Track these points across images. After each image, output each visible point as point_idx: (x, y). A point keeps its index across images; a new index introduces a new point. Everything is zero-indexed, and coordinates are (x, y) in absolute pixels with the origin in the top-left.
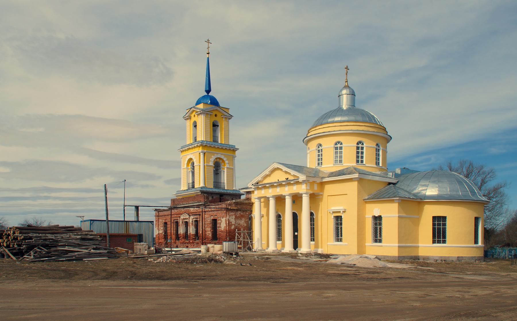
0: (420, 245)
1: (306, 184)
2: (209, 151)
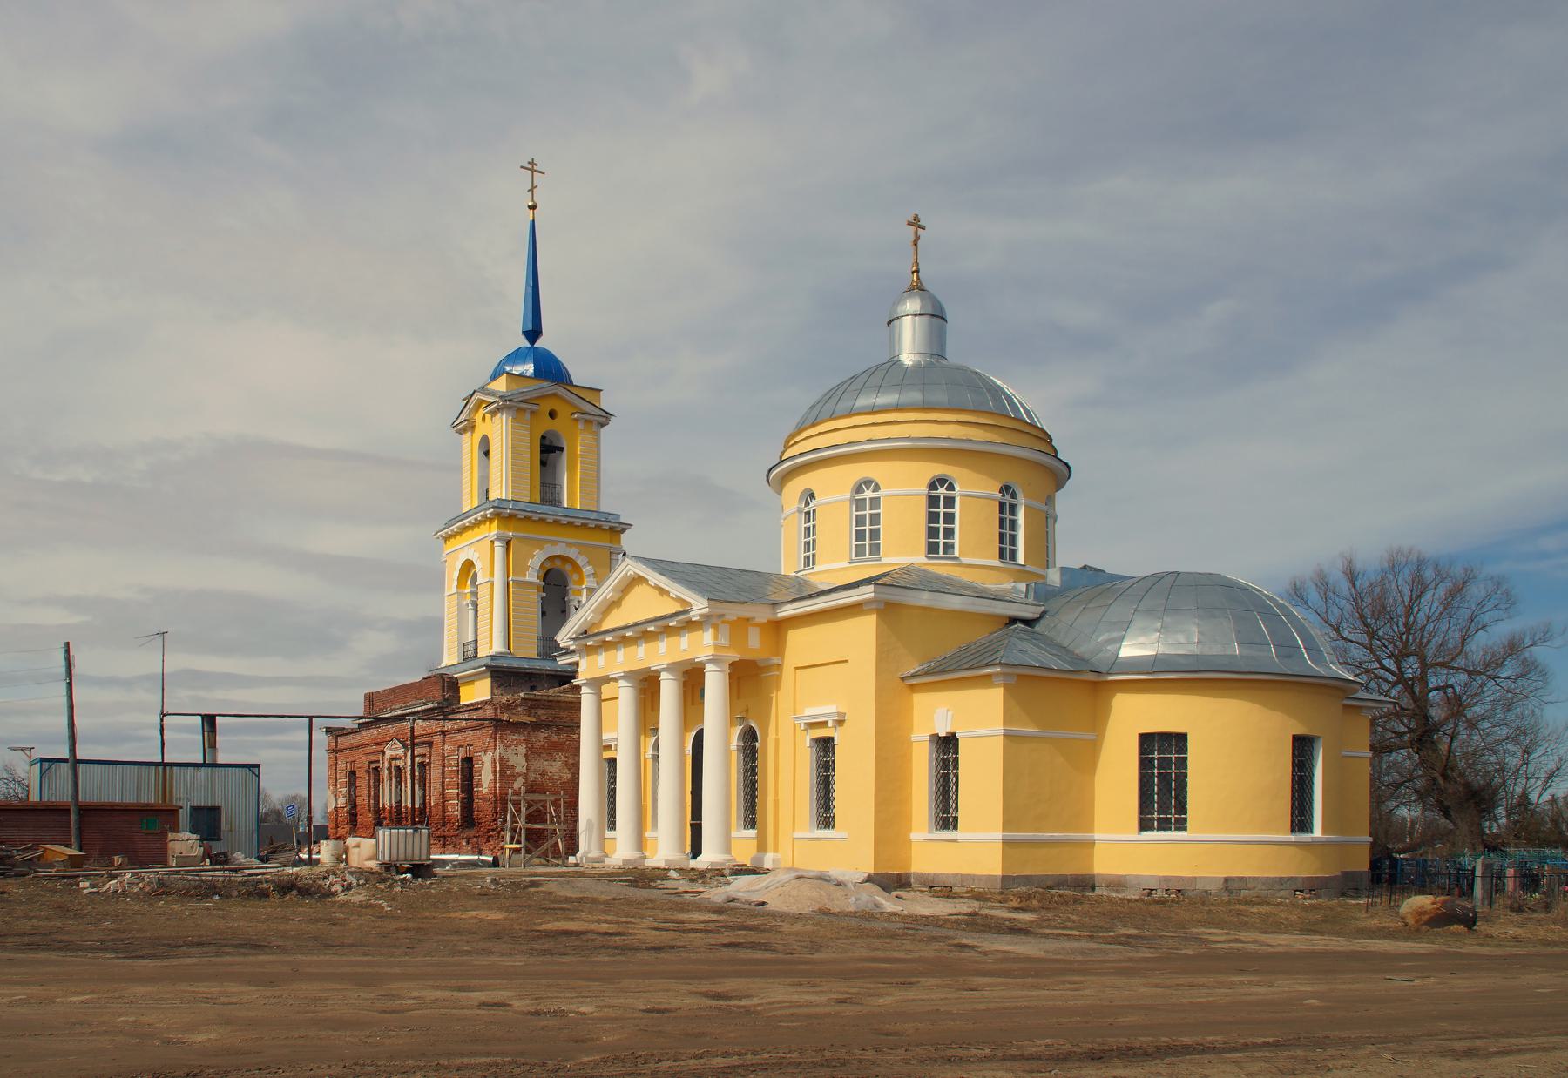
0: (1097, 836)
1: (716, 627)
2: (526, 535)
